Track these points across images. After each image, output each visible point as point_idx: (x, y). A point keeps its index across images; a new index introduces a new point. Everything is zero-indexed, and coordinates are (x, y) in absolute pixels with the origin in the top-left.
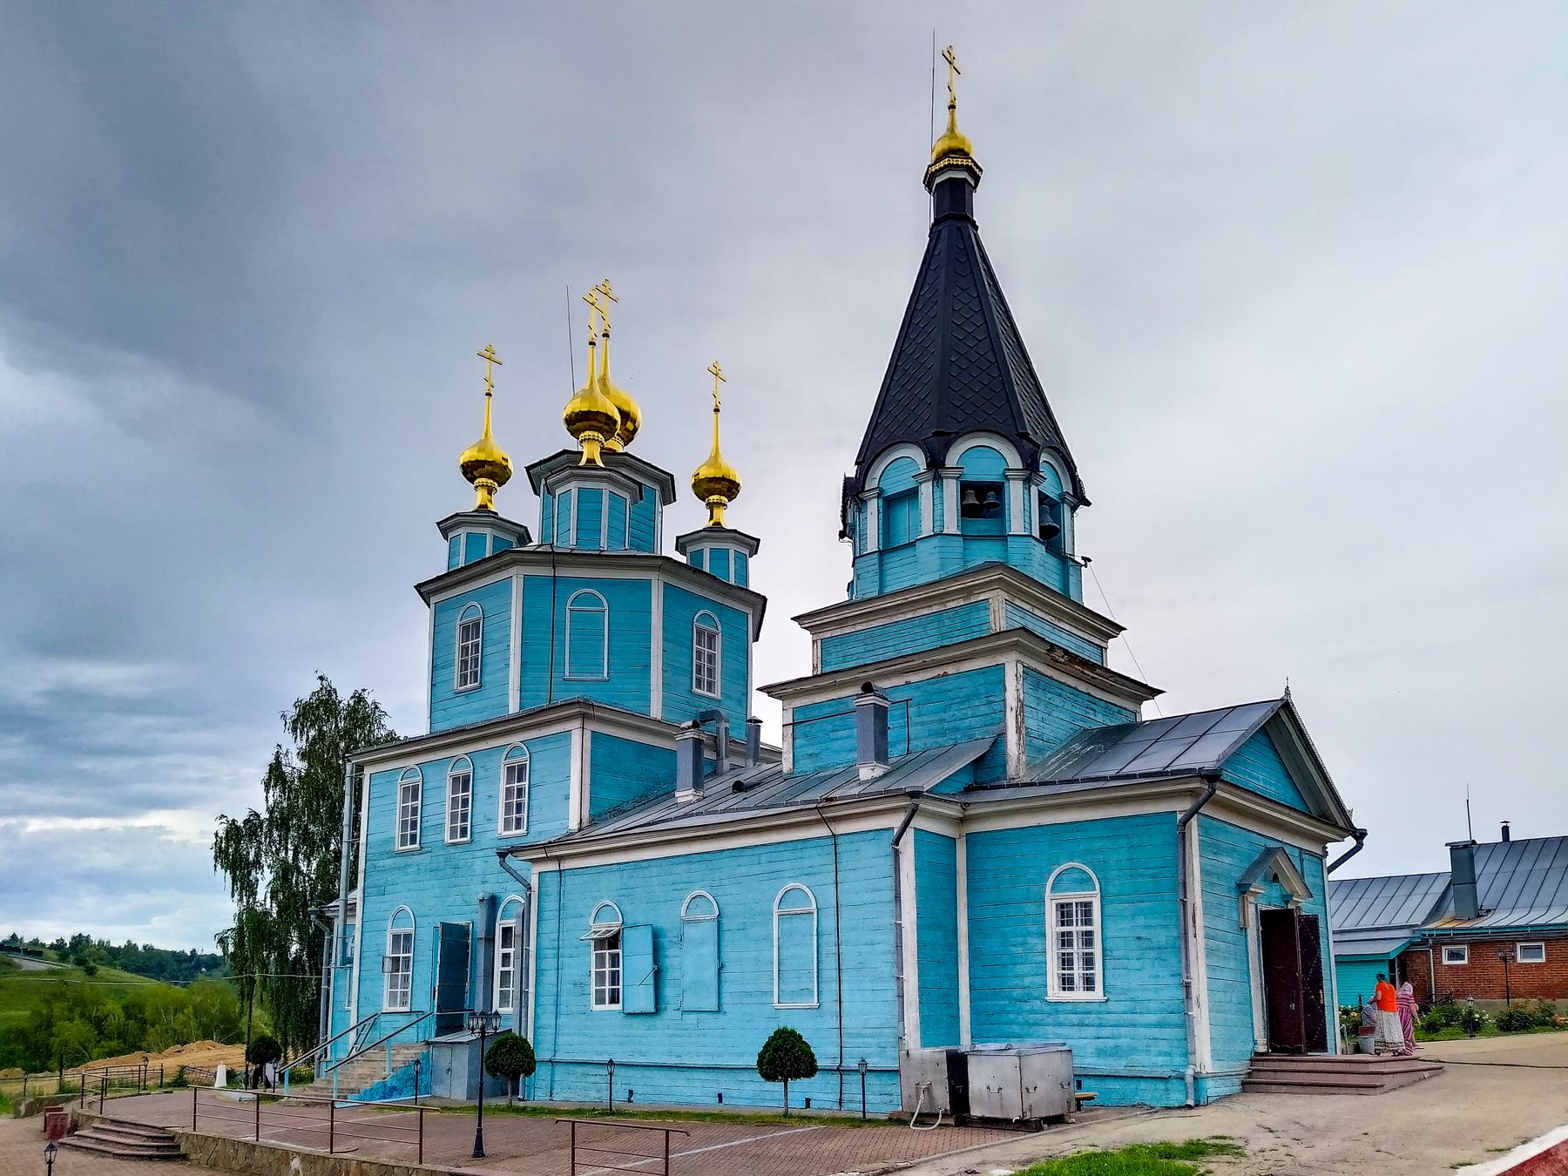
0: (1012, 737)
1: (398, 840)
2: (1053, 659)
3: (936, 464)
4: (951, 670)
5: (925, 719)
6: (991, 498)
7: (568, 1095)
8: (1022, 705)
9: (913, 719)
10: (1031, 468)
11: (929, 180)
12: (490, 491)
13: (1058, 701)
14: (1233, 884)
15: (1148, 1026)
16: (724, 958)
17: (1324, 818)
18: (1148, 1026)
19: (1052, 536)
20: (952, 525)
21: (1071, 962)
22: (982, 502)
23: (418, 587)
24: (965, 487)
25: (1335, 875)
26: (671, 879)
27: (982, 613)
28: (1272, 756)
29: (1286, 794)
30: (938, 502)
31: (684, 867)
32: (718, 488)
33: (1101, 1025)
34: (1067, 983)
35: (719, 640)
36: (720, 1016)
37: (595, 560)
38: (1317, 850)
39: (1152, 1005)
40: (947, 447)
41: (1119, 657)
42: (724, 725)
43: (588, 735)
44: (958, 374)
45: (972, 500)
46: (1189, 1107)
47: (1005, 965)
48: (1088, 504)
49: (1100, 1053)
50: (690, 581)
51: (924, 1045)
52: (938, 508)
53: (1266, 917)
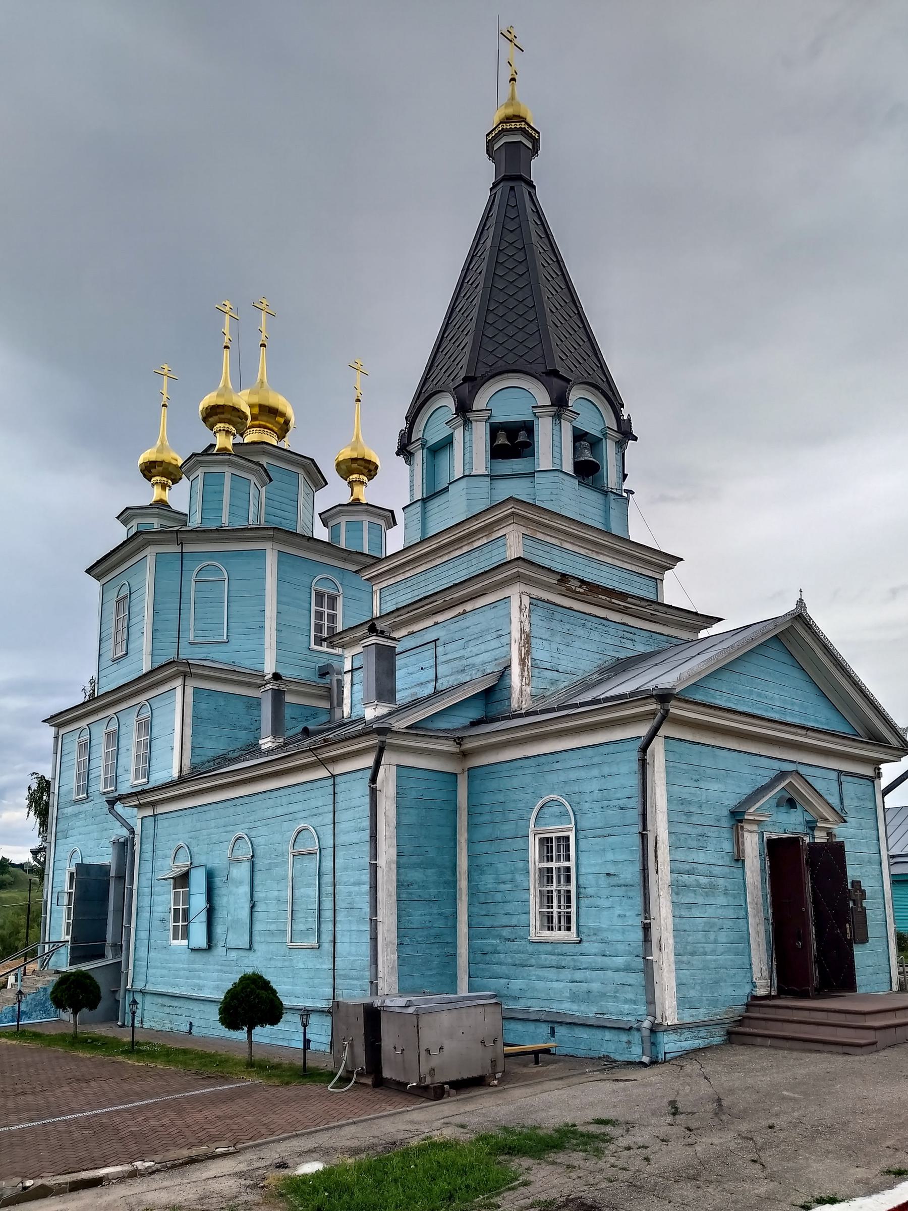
0: (516, 669)
1: (75, 791)
2: (569, 589)
3: (560, 403)
4: (468, 607)
5: (449, 657)
6: (522, 437)
7: (153, 1024)
8: (527, 639)
9: (441, 659)
10: (560, 403)
13: (580, 631)
14: (726, 813)
15: (616, 970)
16: (259, 894)
17: (876, 740)
18: (616, 970)
19: (587, 471)
20: (481, 465)
21: (550, 899)
22: (511, 442)
23: (88, 571)
24: (495, 430)
25: (891, 801)
26: (221, 822)
27: (502, 549)
28: (796, 673)
29: (819, 715)
30: (556, 446)
31: (232, 810)
33: (575, 968)
34: (548, 922)
35: (340, 602)
36: (251, 954)
37: (215, 535)
38: (869, 771)
39: (621, 947)
40: (473, 393)
41: (675, 591)
42: (336, 677)
43: (189, 691)
44: (517, 323)
45: (502, 440)
46: (644, 1065)
47: (497, 903)
48: (635, 439)
49: (574, 997)
50: (308, 549)
51: (402, 991)
52: (472, 449)
53: (780, 852)
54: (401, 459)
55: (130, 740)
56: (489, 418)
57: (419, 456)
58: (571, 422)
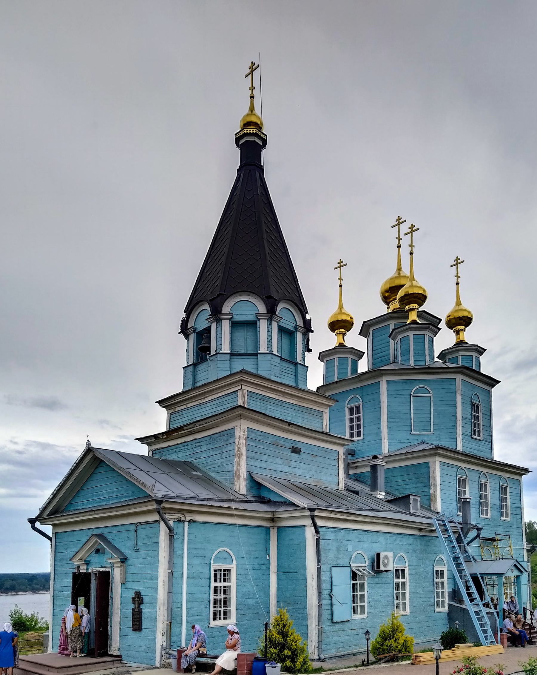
3: (271, 312)
10: (271, 312)
11: (237, 140)
12: (344, 334)
32: (459, 322)
54: (182, 335)
55: (291, 373)
56: (231, 318)
57: (192, 337)
58: (278, 322)
